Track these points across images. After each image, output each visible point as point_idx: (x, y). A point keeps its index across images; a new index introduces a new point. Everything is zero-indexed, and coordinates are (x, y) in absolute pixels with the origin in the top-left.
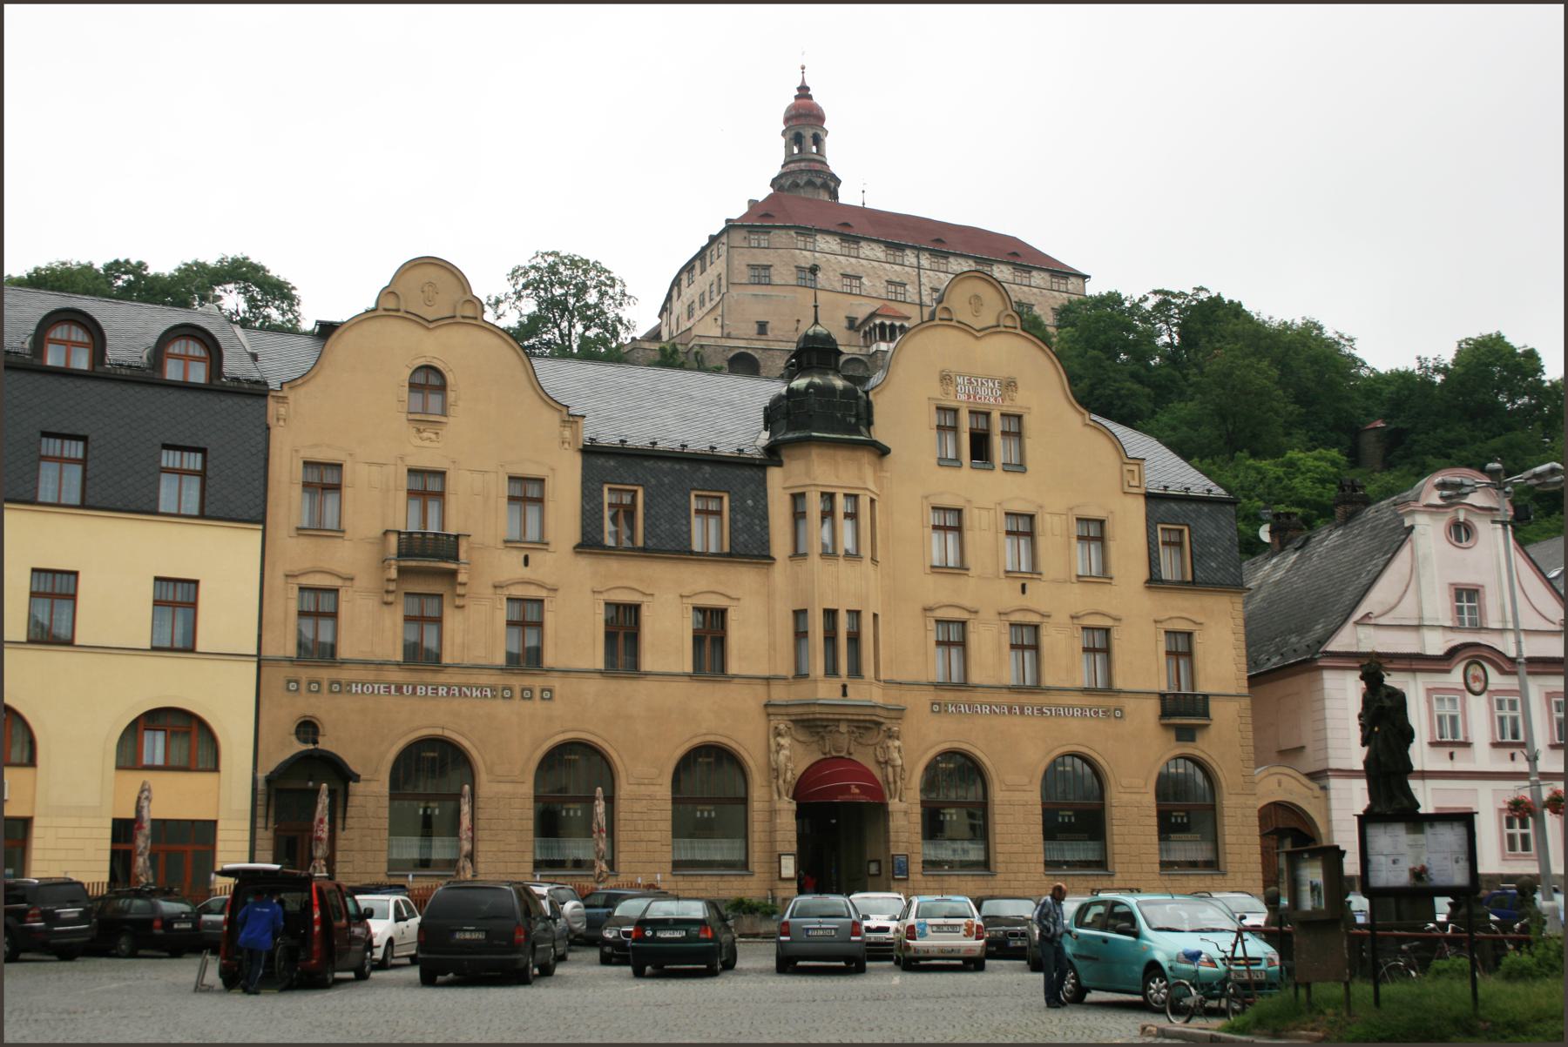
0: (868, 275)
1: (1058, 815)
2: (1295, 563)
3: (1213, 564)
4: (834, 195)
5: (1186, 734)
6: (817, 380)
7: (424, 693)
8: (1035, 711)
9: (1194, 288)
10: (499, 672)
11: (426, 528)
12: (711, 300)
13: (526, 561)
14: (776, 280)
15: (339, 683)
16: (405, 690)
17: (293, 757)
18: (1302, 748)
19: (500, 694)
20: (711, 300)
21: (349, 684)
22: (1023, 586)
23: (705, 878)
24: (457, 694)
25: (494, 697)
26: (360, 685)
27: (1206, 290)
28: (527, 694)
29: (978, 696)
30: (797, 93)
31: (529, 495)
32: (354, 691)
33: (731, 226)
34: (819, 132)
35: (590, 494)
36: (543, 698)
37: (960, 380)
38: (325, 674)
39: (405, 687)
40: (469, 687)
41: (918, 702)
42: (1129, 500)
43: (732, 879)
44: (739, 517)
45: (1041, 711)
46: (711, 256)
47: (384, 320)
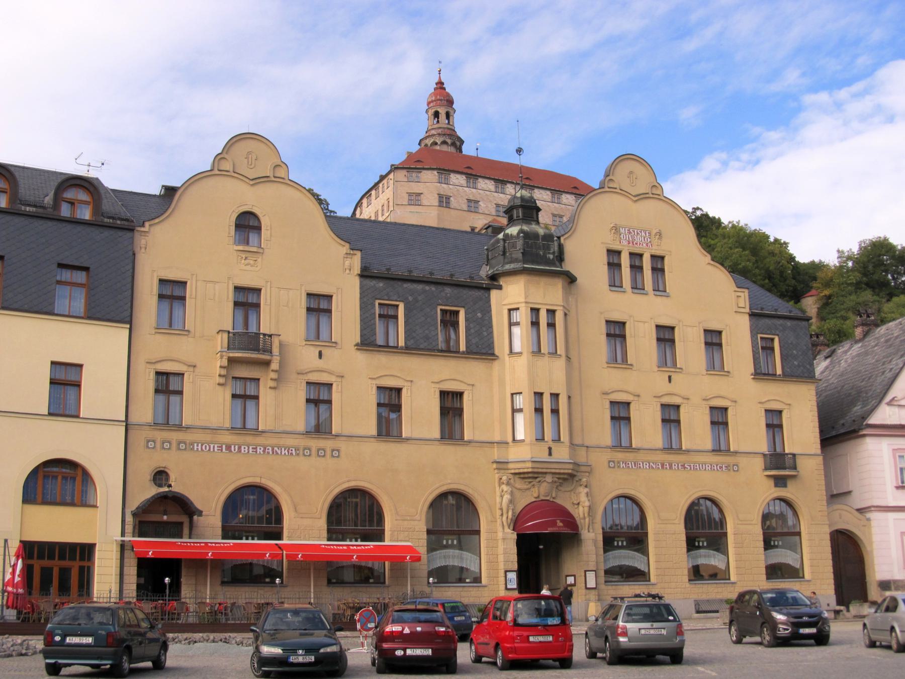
0: (483, 200)
1: (771, 540)
2: (827, 368)
3: (795, 362)
4: (460, 150)
5: (780, 482)
6: (525, 228)
7: (247, 451)
8: (680, 467)
9: (693, 208)
10: (301, 436)
11: (247, 329)
12: (383, 215)
13: (320, 355)
14: (425, 202)
15: (185, 443)
16: (233, 449)
17: (153, 497)
18: (849, 492)
19: (301, 453)
20: (383, 215)
21: (192, 444)
22: (670, 377)
23: (451, 589)
24: (271, 453)
25: (297, 455)
26: (200, 445)
27: (701, 209)
28: (321, 453)
29: (641, 456)
30: (436, 86)
31: (321, 307)
32: (195, 449)
33: (394, 168)
34: (450, 111)
35: (365, 306)
36: (333, 456)
37: (622, 231)
38: (175, 436)
39: (233, 447)
40: (279, 447)
41: (599, 460)
42: (738, 316)
43: (471, 589)
44: (472, 325)
45: (683, 466)
46: (383, 187)
47: (217, 178)
